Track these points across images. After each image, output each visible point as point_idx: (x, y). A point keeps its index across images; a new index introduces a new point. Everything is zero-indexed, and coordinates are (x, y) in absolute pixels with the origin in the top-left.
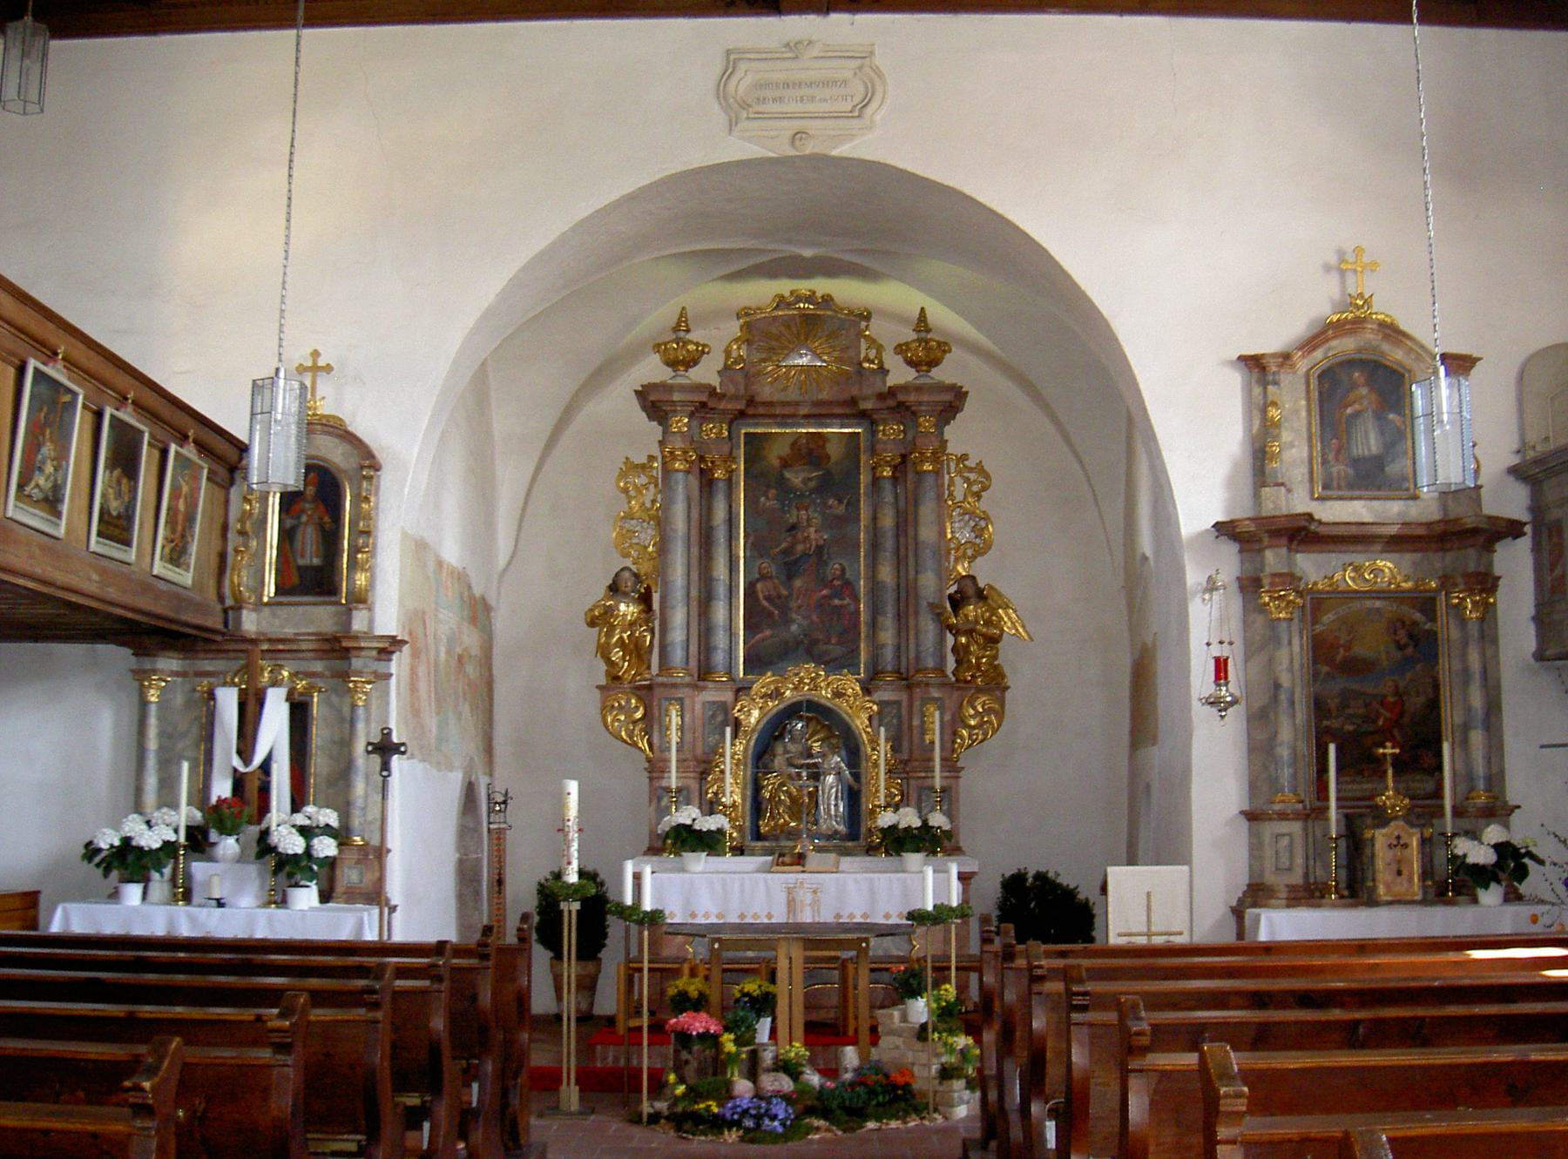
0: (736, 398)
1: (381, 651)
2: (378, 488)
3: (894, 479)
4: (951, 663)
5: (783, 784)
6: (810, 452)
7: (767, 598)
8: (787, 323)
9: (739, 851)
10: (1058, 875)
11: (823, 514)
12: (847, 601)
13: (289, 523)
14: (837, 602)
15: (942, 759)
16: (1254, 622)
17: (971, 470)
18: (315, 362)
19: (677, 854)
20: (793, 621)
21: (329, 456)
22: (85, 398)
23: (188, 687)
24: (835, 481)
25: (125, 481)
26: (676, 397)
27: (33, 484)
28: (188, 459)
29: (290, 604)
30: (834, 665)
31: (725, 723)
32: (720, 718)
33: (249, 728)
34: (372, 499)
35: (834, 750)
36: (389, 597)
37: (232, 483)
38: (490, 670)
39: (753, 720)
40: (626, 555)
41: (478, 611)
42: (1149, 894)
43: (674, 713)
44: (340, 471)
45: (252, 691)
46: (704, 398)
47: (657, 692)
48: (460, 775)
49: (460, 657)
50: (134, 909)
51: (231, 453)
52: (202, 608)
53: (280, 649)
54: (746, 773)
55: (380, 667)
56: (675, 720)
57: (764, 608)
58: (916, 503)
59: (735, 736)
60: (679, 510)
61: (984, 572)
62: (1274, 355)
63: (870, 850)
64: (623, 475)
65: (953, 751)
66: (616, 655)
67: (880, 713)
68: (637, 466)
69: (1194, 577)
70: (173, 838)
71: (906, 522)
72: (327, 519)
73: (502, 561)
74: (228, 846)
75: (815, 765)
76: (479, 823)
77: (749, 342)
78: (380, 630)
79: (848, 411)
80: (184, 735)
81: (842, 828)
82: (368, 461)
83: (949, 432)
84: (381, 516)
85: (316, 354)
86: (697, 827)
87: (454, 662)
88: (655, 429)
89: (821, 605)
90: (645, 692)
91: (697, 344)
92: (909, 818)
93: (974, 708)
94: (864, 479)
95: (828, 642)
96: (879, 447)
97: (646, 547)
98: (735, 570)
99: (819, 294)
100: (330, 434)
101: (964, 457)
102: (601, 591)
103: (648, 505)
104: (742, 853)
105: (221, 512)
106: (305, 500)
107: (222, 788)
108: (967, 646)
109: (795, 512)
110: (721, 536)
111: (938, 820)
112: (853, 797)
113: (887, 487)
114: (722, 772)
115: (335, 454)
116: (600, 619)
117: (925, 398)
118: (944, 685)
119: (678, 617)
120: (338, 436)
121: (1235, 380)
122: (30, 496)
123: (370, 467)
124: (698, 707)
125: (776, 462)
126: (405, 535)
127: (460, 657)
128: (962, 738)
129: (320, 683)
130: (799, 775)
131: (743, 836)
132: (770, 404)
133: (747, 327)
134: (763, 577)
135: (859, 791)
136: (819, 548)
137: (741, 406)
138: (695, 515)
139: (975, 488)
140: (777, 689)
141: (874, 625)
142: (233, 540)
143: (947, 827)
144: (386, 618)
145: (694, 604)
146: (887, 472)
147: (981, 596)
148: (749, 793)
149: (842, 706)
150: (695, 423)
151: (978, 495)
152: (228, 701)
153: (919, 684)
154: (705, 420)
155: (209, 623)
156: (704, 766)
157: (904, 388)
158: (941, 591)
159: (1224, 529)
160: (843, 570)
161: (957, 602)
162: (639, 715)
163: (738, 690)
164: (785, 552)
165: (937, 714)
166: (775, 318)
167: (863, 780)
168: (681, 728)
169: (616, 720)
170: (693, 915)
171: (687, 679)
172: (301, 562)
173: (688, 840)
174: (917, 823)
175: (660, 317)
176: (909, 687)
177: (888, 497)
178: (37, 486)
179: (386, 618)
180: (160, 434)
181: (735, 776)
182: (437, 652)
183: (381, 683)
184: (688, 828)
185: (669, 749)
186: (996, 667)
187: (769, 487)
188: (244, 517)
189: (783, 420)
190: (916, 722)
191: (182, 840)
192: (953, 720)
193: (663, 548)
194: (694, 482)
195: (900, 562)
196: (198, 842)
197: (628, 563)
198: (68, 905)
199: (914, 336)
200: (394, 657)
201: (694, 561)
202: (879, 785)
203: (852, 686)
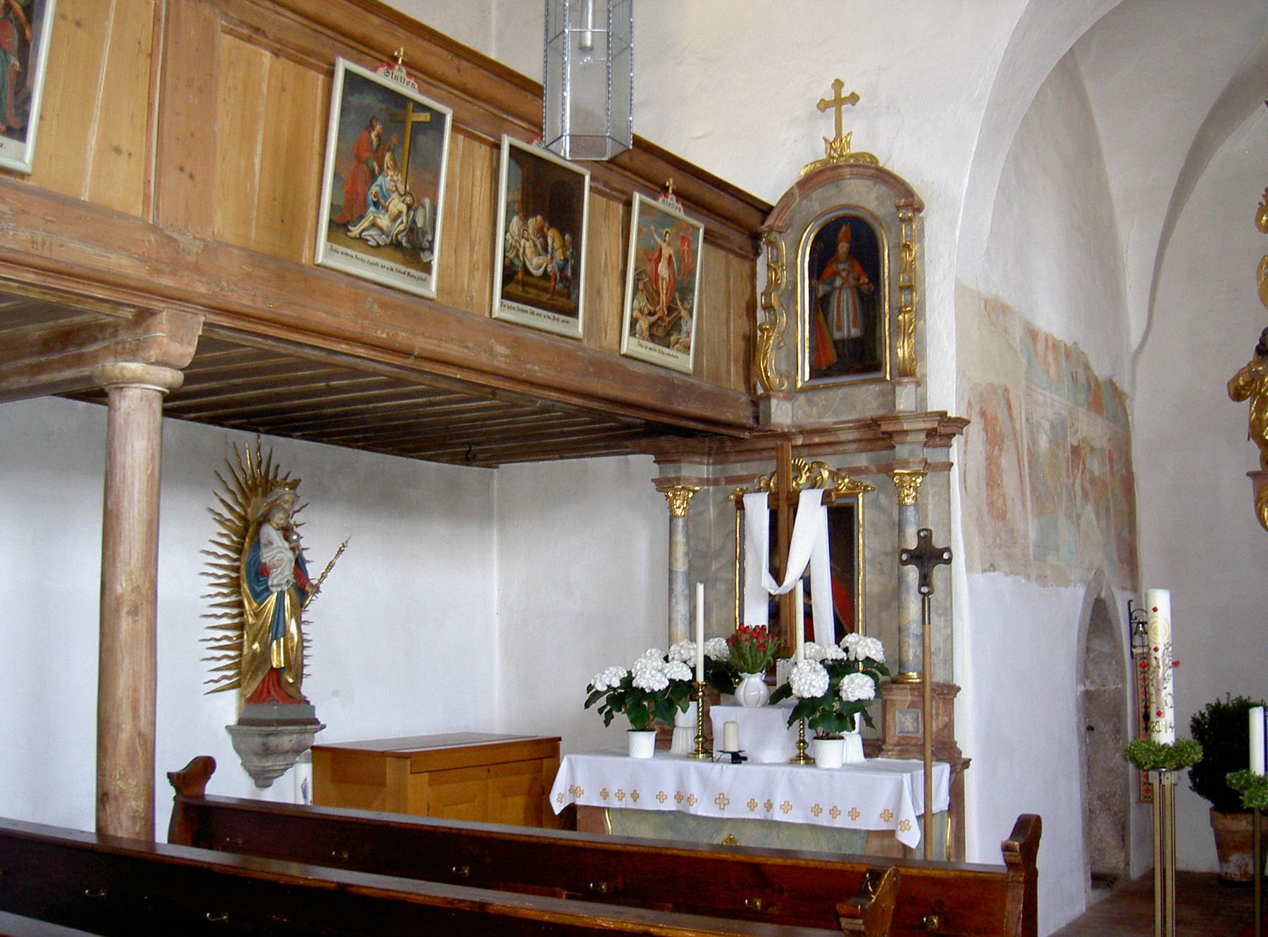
1: (931, 433)
2: (922, 231)
13: (822, 290)
18: (838, 93)
21: (862, 204)
22: (592, 179)
23: (720, 496)
25: (552, 234)
27: (365, 223)
28: (667, 215)
29: (826, 387)
33: (782, 541)
34: (915, 248)
36: (944, 363)
37: (757, 254)
38: (1128, 465)
41: (1105, 398)
44: (876, 218)
45: (783, 496)
48: (1081, 591)
49: (1076, 451)
50: (642, 763)
51: (751, 217)
52: (718, 398)
53: (817, 440)
55: (935, 455)
70: (688, 676)
72: (864, 280)
73: (1135, 338)
74: (753, 685)
76: (1120, 648)
78: (934, 405)
80: (718, 553)
82: (908, 201)
84: (929, 270)
85: (838, 84)
100: (862, 176)
105: (749, 289)
106: (838, 261)
107: (757, 616)
115: (863, 197)
120: (872, 177)
122: (360, 238)
123: (907, 206)
126: (961, 291)
127: (1076, 451)
129: (867, 481)
142: (760, 315)
144: (943, 390)
152: (758, 508)
155: (729, 416)
172: (837, 335)
178: (374, 225)
179: (943, 390)
180: (475, 110)
182: (1034, 442)
183: (939, 477)
188: (772, 285)
191: (700, 678)
196: (722, 679)
198: (573, 757)
200: (955, 441)
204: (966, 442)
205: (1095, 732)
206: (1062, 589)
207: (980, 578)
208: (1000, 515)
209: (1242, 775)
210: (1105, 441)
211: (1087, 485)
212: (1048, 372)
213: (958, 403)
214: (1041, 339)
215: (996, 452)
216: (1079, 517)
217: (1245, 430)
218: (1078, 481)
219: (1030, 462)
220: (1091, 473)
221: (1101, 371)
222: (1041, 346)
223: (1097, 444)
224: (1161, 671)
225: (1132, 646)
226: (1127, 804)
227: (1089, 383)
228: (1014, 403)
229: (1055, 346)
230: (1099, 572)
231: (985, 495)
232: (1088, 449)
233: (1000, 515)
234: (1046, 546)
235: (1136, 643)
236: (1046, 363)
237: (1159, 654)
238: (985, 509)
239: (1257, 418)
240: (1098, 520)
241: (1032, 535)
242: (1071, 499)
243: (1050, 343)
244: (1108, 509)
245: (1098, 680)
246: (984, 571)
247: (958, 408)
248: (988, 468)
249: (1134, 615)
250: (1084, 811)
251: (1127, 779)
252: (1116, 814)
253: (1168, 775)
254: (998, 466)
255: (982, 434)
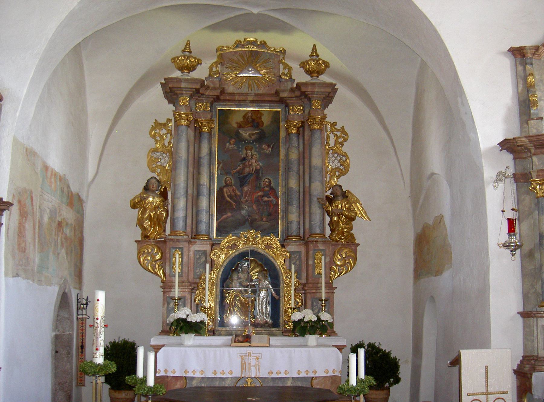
0: (215, 89)
3: (298, 133)
4: (328, 232)
5: (236, 296)
6: (253, 120)
7: (228, 196)
8: (242, 55)
9: (213, 333)
10: (380, 344)
11: (259, 152)
12: (272, 198)
14: (266, 199)
15: (326, 283)
16: (524, 199)
17: (338, 130)
19: (178, 335)
20: (243, 209)
24: (266, 135)
26: (183, 85)
30: (265, 232)
31: (206, 262)
32: (203, 259)
35: (265, 278)
38: (82, 233)
39: (221, 261)
40: (153, 171)
41: (75, 201)
42: (487, 367)
43: (177, 256)
46: (198, 86)
47: (169, 244)
48: (57, 288)
49: (60, 224)
54: (216, 290)
56: (178, 259)
57: (228, 202)
58: (310, 146)
59: (211, 269)
60: (183, 146)
61: (345, 183)
62: (531, 48)
63: (285, 333)
64: (153, 128)
65: (330, 278)
66: (147, 223)
67: (290, 257)
68: (161, 124)
69: (489, 173)
71: (305, 156)
73: (90, 176)
75: (254, 285)
76: (71, 315)
77: (222, 64)
79: (274, 99)
81: (269, 320)
83: (326, 111)
86: (189, 320)
87: (55, 225)
88: (172, 107)
89: (258, 201)
90: (162, 245)
91: (195, 58)
92: (309, 315)
93: (341, 255)
94: (282, 134)
95: (262, 220)
96: (290, 118)
97: (165, 167)
98: (211, 180)
99: (259, 41)
101: (334, 124)
102: (140, 190)
103: (166, 144)
104: (214, 334)
108: (338, 222)
109: (245, 151)
110: (205, 161)
111: (325, 316)
112: (275, 303)
113: (295, 138)
114: (204, 289)
116: (137, 204)
117: (316, 90)
118: (325, 242)
119: (181, 203)
121: (505, 66)
124: (191, 254)
125: (235, 126)
126: (16, 142)
127: (60, 224)
128: (335, 272)
130: (246, 291)
131: (214, 324)
132: (232, 94)
133: (221, 57)
134: (227, 185)
135: (279, 300)
136: (257, 172)
137: (217, 93)
138: (191, 150)
139: (340, 140)
140: (234, 244)
141: (286, 211)
143: (330, 321)
145: (190, 198)
146: (294, 130)
147: (345, 195)
148: (218, 300)
149: (269, 254)
150: (192, 102)
151: (342, 144)
153: (312, 242)
154: (197, 101)
156: (194, 286)
157: (306, 84)
158: (323, 192)
159: (506, 145)
160: (270, 183)
161: (330, 200)
162: (158, 257)
163: (213, 245)
164: (238, 172)
165: (323, 258)
166: (236, 52)
167: (281, 294)
168: (181, 264)
169: (145, 259)
170: (186, 372)
171: (186, 237)
173: (184, 327)
174: (314, 318)
175: (174, 47)
176: (306, 244)
177: (295, 143)
181: (211, 290)
182: (42, 217)
184: (184, 320)
185: (174, 276)
186: (352, 235)
187: (231, 138)
189: (239, 103)
190: (310, 262)
192: (330, 262)
193: (174, 168)
194: (191, 133)
195: (301, 178)
197: (155, 175)
199: (309, 58)
201: (190, 176)
202: (290, 296)
203: (275, 242)
204: (10, 214)
205: (58, 354)
206: (48, 287)
207: (11, 280)
208: (23, 250)
209: (133, 378)
210: (73, 220)
211: (64, 240)
212: (51, 186)
213: (8, 195)
214: (50, 170)
215: (24, 221)
216: (58, 254)
217: (136, 221)
218: (59, 238)
219: (39, 227)
220: (66, 235)
221: (74, 189)
222: (49, 173)
223: (70, 222)
224: (99, 329)
225: (78, 315)
226: (71, 386)
227: (68, 193)
228: (34, 198)
229: (55, 174)
230: (66, 280)
231: (16, 239)
232: (65, 223)
233: (23, 250)
234: (43, 266)
235: (79, 313)
236: (51, 182)
237: (99, 321)
238: (16, 247)
239: (141, 217)
240: (67, 256)
241: (37, 261)
242: (56, 245)
243: (53, 173)
244: (71, 252)
245: (61, 330)
246: (13, 276)
247: (8, 197)
248: (19, 228)
249: (79, 300)
250: (52, 390)
251: (72, 375)
252: (66, 391)
253: (100, 378)
254: (24, 227)
255: (18, 211)
